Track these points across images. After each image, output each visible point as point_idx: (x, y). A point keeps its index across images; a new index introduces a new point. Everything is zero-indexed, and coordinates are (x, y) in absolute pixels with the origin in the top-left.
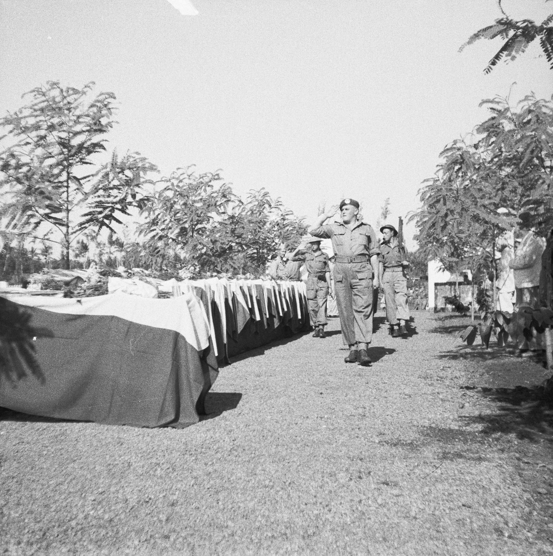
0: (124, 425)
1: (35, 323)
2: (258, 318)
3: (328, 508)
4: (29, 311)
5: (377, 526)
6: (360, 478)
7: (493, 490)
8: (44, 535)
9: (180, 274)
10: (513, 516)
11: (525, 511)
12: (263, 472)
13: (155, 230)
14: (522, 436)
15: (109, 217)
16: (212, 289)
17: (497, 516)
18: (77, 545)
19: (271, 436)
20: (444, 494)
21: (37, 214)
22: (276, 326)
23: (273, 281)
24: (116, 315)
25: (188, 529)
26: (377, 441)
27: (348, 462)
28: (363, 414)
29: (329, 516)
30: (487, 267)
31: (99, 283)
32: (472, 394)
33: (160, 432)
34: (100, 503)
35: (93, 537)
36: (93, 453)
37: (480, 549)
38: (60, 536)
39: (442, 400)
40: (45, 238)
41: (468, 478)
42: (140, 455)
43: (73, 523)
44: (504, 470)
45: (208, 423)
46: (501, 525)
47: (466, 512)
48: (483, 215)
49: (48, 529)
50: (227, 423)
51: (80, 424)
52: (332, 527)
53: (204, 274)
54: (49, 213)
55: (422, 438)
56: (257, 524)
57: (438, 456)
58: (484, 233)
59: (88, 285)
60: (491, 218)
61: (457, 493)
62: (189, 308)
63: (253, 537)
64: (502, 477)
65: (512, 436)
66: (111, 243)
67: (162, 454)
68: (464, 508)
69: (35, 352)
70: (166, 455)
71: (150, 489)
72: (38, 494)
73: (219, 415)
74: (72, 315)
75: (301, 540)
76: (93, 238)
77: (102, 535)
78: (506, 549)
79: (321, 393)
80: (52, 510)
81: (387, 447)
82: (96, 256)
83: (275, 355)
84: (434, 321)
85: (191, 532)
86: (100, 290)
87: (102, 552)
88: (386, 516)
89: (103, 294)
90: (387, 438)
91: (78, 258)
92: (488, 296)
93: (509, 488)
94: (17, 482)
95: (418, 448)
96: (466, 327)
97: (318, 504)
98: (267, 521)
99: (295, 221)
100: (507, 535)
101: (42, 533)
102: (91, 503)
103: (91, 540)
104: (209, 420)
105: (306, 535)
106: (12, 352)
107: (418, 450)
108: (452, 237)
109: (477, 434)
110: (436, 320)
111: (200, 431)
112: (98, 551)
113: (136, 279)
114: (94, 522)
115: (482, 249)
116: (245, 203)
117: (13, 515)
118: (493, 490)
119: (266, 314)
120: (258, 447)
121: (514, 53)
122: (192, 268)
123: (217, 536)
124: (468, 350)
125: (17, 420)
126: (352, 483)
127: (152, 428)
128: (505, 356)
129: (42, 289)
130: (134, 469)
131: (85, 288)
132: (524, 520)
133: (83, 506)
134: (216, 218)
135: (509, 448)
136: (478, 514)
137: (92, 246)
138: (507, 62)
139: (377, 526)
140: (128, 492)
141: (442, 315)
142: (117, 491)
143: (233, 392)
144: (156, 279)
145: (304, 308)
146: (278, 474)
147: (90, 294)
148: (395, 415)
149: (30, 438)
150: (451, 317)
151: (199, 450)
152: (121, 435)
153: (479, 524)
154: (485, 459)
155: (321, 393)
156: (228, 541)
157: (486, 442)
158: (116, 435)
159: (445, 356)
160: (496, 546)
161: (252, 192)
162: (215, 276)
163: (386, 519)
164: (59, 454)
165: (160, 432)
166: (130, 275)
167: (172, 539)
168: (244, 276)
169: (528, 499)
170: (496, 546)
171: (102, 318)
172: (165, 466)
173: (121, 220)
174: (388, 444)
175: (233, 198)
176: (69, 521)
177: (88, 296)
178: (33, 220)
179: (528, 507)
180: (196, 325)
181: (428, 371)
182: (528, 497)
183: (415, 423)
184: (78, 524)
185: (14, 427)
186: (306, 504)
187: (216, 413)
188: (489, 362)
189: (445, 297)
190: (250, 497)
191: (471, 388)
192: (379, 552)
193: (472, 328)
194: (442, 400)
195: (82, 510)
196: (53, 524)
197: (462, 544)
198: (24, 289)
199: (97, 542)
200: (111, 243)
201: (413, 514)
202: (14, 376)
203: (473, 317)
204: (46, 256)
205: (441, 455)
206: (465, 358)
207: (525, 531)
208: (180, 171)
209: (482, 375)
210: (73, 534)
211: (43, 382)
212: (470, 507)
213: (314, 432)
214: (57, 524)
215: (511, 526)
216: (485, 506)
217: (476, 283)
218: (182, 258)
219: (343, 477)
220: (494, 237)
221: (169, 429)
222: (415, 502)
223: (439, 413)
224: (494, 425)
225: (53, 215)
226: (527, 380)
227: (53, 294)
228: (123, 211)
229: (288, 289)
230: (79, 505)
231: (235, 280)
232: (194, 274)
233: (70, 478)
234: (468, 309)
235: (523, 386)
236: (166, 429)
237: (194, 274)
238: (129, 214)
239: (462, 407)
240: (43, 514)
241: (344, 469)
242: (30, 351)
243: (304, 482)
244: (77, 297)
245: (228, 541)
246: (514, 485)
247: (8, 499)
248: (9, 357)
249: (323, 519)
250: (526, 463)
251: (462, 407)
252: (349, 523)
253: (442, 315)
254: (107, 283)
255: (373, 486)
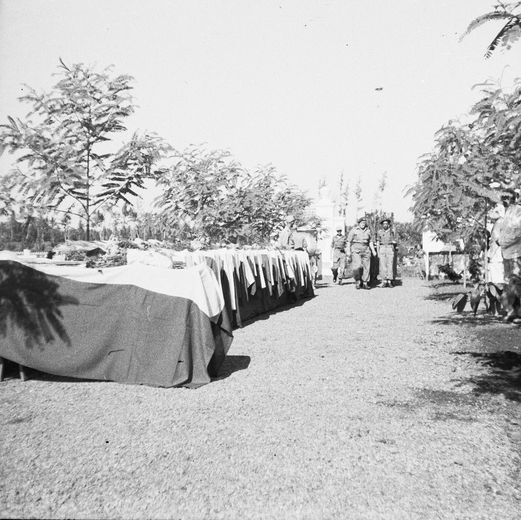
0: (142, 384)
1: (61, 291)
2: (263, 286)
3: (330, 464)
4: (56, 281)
5: (375, 481)
6: (360, 436)
7: (483, 448)
8: (73, 485)
9: (192, 245)
10: (502, 474)
11: (512, 468)
12: (270, 430)
13: (170, 202)
14: (511, 397)
15: (126, 190)
16: (222, 259)
17: (487, 473)
18: (104, 495)
19: (277, 396)
20: (437, 452)
21: (61, 189)
22: (280, 295)
23: (278, 251)
24: (134, 284)
25: (203, 482)
26: (375, 402)
27: (349, 421)
28: (362, 376)
29: (331, 471)
30: (478, 237)
31: (119, 255)
32: (463, 359)
33: (175, 392)
34: (122, 457)
35: (118, 488)
36: (114, 411)
37: (470, 503)
38: (87, 487)
39: (435, 364)
40: (66, 212)
41: (459, 437)
42: (157, 414)
43: (99, 475)
44: (494, 431)
45: (219, 383)
46: (490, 482)
47: (458, 470)
48: (475, 188)
49: (77, 480)
50: (237, 383)
51: (102, 383)
52: (334, 481)
53: (214, 245)
54: (73, 189)
55: (417, 399)
56: (266, 478)
57: (432, 416)
58: (476, 205)
59: (109, 256)
60: (483, 192)
61: (449, 451)
62: (202, 278)
63: (262, 490)
64: (491, 437)
65: (501, 397)
66: (126, 213)
67: (177, 413)
68: (456, 465)
69: (62, 317)
70: (182, 413)
71: (167, 445)
72: (65, 448)
73: (229, 376)
74: (95, 284)
75: (306, 493)
76: (109, 209)
77: (125, 486)
78: (494, 503)
79: (323, 357)
80: (80, 462)
81: (384, 407)
82: (111, 226)
83: (279, 320)
84: (428, 289)
85: (206, 484)
86: (119, 261)
87: (126, 501)
88: (383, 471)
89: (122, 264)
90: (383, 399)
91: (95, 227)
92: (481, 266)
93: (498, 447)
94: (46, 437)
95: (413, 409)
96: (457, 294)
97: (321, 459)
98: (275, 475)
99: (298, 194)
100: (495, 490)
101: (71, 484)
102: (114, 457)
103: (116, 490)
104: (220, 381)
105: (310, 488)
106: (41, 317)
107: (414, 411)
108: (446, 209)
109: (468, 396)
110: (430, 287)
111: (212, 391)
112: (122, 501)
113: (152, 250)
114: (118, 474)
115: (474, 221)
116: (253, 177)
117: (45, 466)
118: (483, 448)
119: (271, 282)
120: (265, 406)
121: (509, 43)
122: (203, 239)
123: (230, 488)
124: (460, 316)
125: (44, 379)
126: (352, 441)
127: (167, 388)
128: (495, 322)
129: (66, 259)
130: (153, 425)
131: (105, 259)
132: (512, 477)
133: (107, 459)
134: (224, 192)
135: (498, 410)
136: (468, 471)
137: (107, 216)
138: (503, 52)
139: (375, 481)
140: (147, 447)
141: (435, 282)
142: (138, 446)
143: (241, 355)
144: (170, 250)
145: (306, 275)
146: (284, 431)
147: (110, 265)
148: (391, 377)
149: (56, 397)
150: (444, 284)
151: (211, 409)
152: (141, 394)
153: (469, 480)
154: (476, 420)
155: (323, 357)
156: (239, 493)
157: (476, 404)
158: (135, 394)
159: (438, 321)
160: (486, 501)
161: (259, 166)
162: (225, 247)
163: (383, 475)
164: (84, 411)
165: (175, 392)
166: (146, 247)
167: (188, 491)
168: (250, 247)
169: (516, 458)
170: (486, 501)
171: (120, 287)
172: (181, 424)
173: (136, 193)
174: (385, 404)
175: (241, 173)
176: (96, 472)
177: (108, 267)
178: (58, 195)
179: (516, 465)
180: (208, 296)
181: (422, 336)
182: (516, 456)
183: (411, 386)
184: (103, 476)
185: (41, 386)
186: (310, 460)
187: (225, 374)
188: (480, 328)
189: (438, 266)
190: (259, 453)
191: (462, 353)
192: (377, 505)
193: (463, 296)
194: (435, 364)
195: (107, 462)
196: (81, 475)
197: (453, 498)
198: (50, 260)
199: (121, 492)
200: (126, 213)
201: (409, 470)
202: (43, 340)
203: (465, 285)
204: (65, 225)
205: (434, 416)
206: (457, 323)
207: (512, 488)
208: (192, 148)
209: (473, 340)
210: (100, 484)
211: (69, 344)
212: (461, 465)
213: (316, 393)
214: (84, 476)
215: (499, 482)
216: (475, 464)
217: (468, 253)
218: (191, 227)
219: (343, 435)
220: (486, 210)
221: (183, 389)
222: (411, 460)
223: (432, 377)
224: (484, 386)
225: (76, 190)
226: (516, 346)
227: (77, 264)
228: (139, 184)
229: (292, 258)
230: (104, 458)
231: (243, 250)
232: (204, 244)
233: (94, 434)
234: (460, 277)
235: (512, 351)
236: (180, 388)
237: (204, 244)
238: (143, 188)
239: (455, 371)
240: (72, 466)
241: (345, 428)
242: (57, 317)
243: (308, 439)
244: (98, 267)
245: (239, 493)
246: (503, 444)
247: (39, 452)
248: (38, 323)
249: (326, 474)
250: (514, 424)
251: (455, 371)
252: (350, 478)
253: (435, 282)
254: (126, 254)
255: (371, 444)
